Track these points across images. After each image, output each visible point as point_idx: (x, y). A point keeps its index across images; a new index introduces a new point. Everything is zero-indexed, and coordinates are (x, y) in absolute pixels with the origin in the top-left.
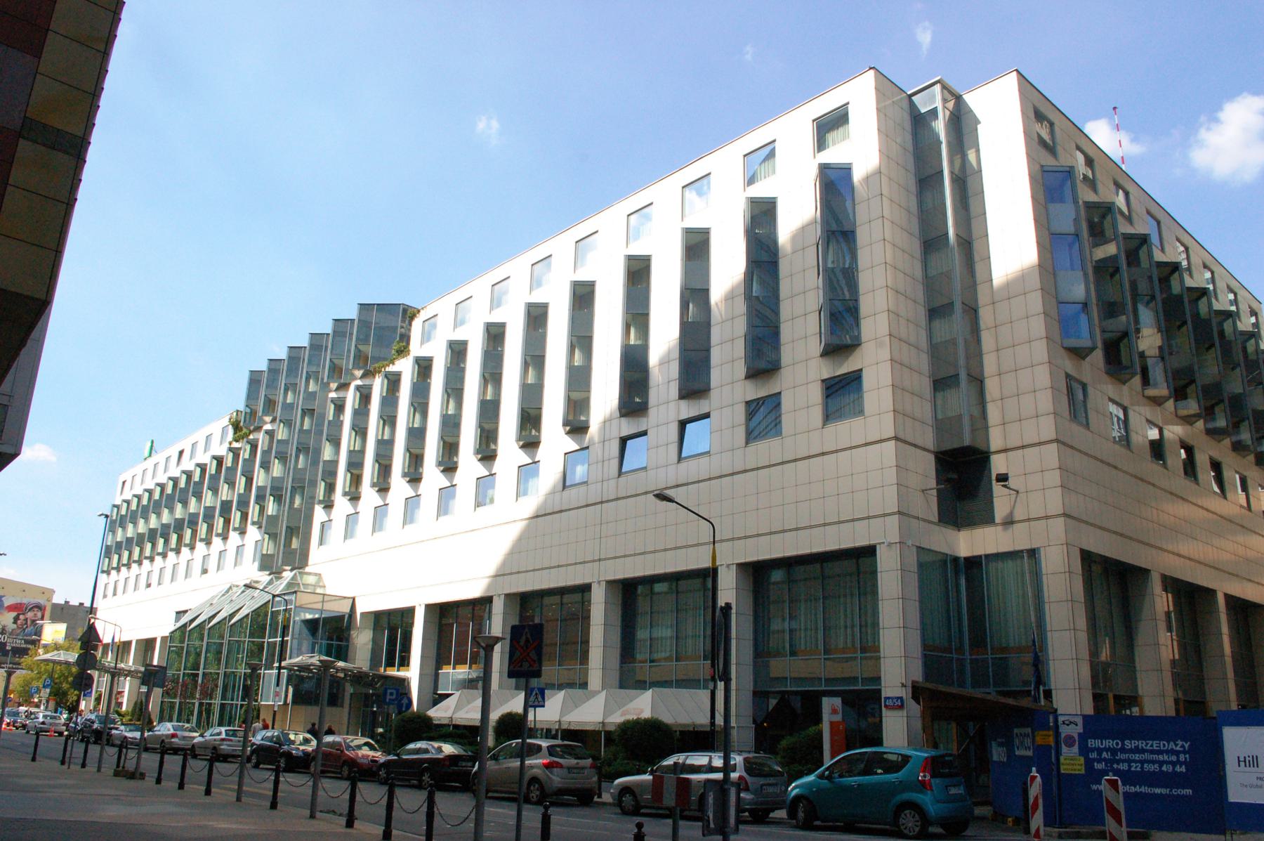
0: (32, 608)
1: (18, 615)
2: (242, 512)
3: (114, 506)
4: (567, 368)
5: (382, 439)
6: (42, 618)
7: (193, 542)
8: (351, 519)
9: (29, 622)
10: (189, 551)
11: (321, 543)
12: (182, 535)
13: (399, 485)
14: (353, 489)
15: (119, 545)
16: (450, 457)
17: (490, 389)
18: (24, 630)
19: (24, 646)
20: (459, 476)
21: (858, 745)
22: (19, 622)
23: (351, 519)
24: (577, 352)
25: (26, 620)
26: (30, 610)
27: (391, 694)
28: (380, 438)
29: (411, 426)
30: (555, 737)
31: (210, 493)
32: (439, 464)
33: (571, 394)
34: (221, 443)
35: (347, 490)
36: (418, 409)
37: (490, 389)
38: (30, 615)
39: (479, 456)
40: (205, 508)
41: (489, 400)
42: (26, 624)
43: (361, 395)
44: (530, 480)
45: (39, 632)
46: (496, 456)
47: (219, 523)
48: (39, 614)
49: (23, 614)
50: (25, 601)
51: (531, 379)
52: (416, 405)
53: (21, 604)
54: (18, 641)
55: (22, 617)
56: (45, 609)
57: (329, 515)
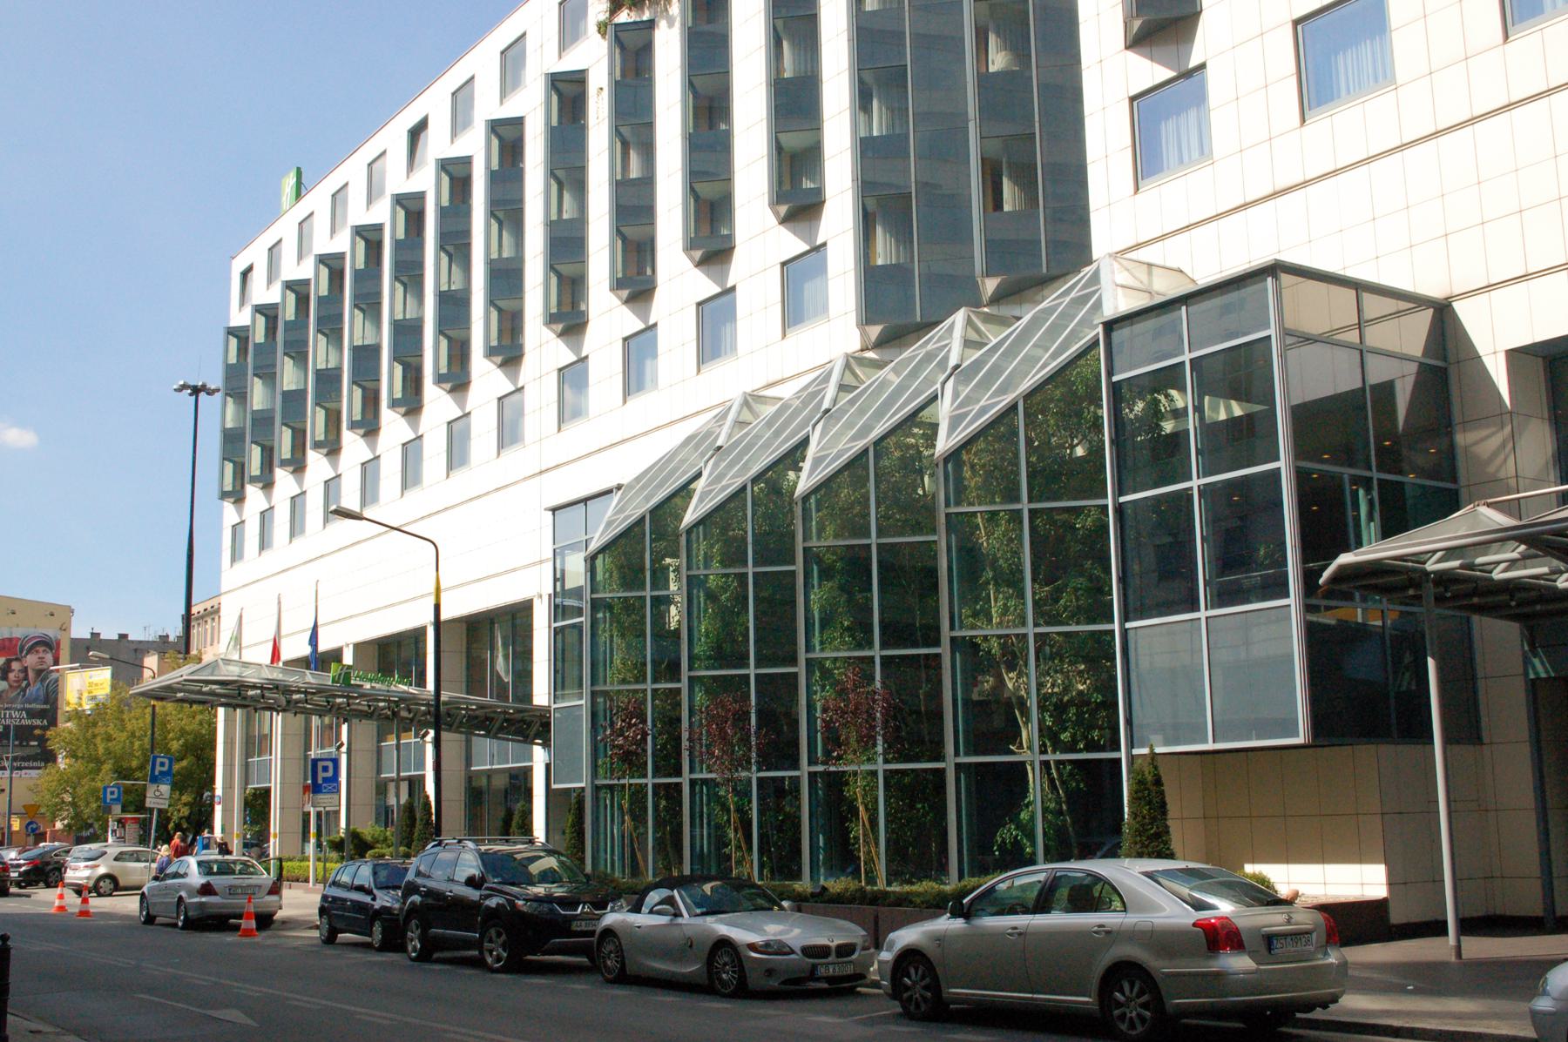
0: (37, 644)
1: (8, 662)
2: (293, 429)
3: (231, 332)
4: (769, 85)
5: (500, 258)
6: (56, 662)
7: (299, 455)
8: (573, 376)
9: (31, 674)
10: (291, 478)
11: (234, 559)
12: (243, 465)
13: (486, 375)
14: (456, 369)
15: (263, 422)
16: (714, 230)
17: (634, 159)
18: (24, 690)
19: (28, 722)
20: (740, 268)
21: (1076, 851)
22: (11, 676)
23: (573, 376)
24: (785, 44)
25: (25, 670)
26: (29, 651)
27: (162, 764)
28: (554, 217)
29: (554, 217)
30: (669, 863)
31: (322, 340)
32: (690, 245)
33: (783, 137)
34: (333, 231)
35: (494, 343)
36: (505, 224)
37: (634, 159)
38: (31, 660)
39: (698, 254)
40: (318, 373)
41: (873, 13)
42: (26, 678)
43: (452, 179)
44: (806, 286)
45: (52, 697)
46: (732, 248)
47: (350, 400)
48: (49, 657)
49: (17, 659)
50: (18, 633)
51: (635, 172)
52: (500, 215)
53: (10, 640)
54: (16, 714)
55: (15, 666)
56: (58, 643)
57: (462, 404)
